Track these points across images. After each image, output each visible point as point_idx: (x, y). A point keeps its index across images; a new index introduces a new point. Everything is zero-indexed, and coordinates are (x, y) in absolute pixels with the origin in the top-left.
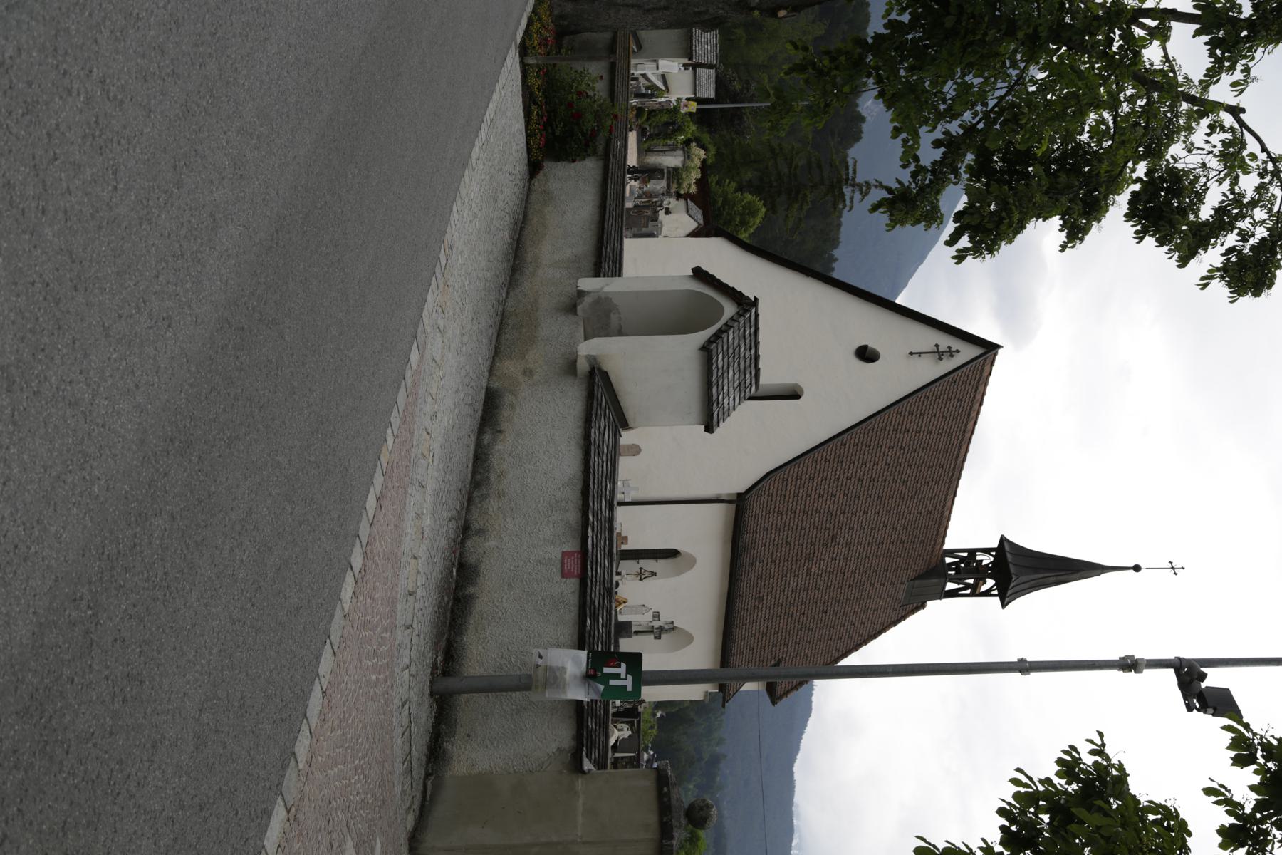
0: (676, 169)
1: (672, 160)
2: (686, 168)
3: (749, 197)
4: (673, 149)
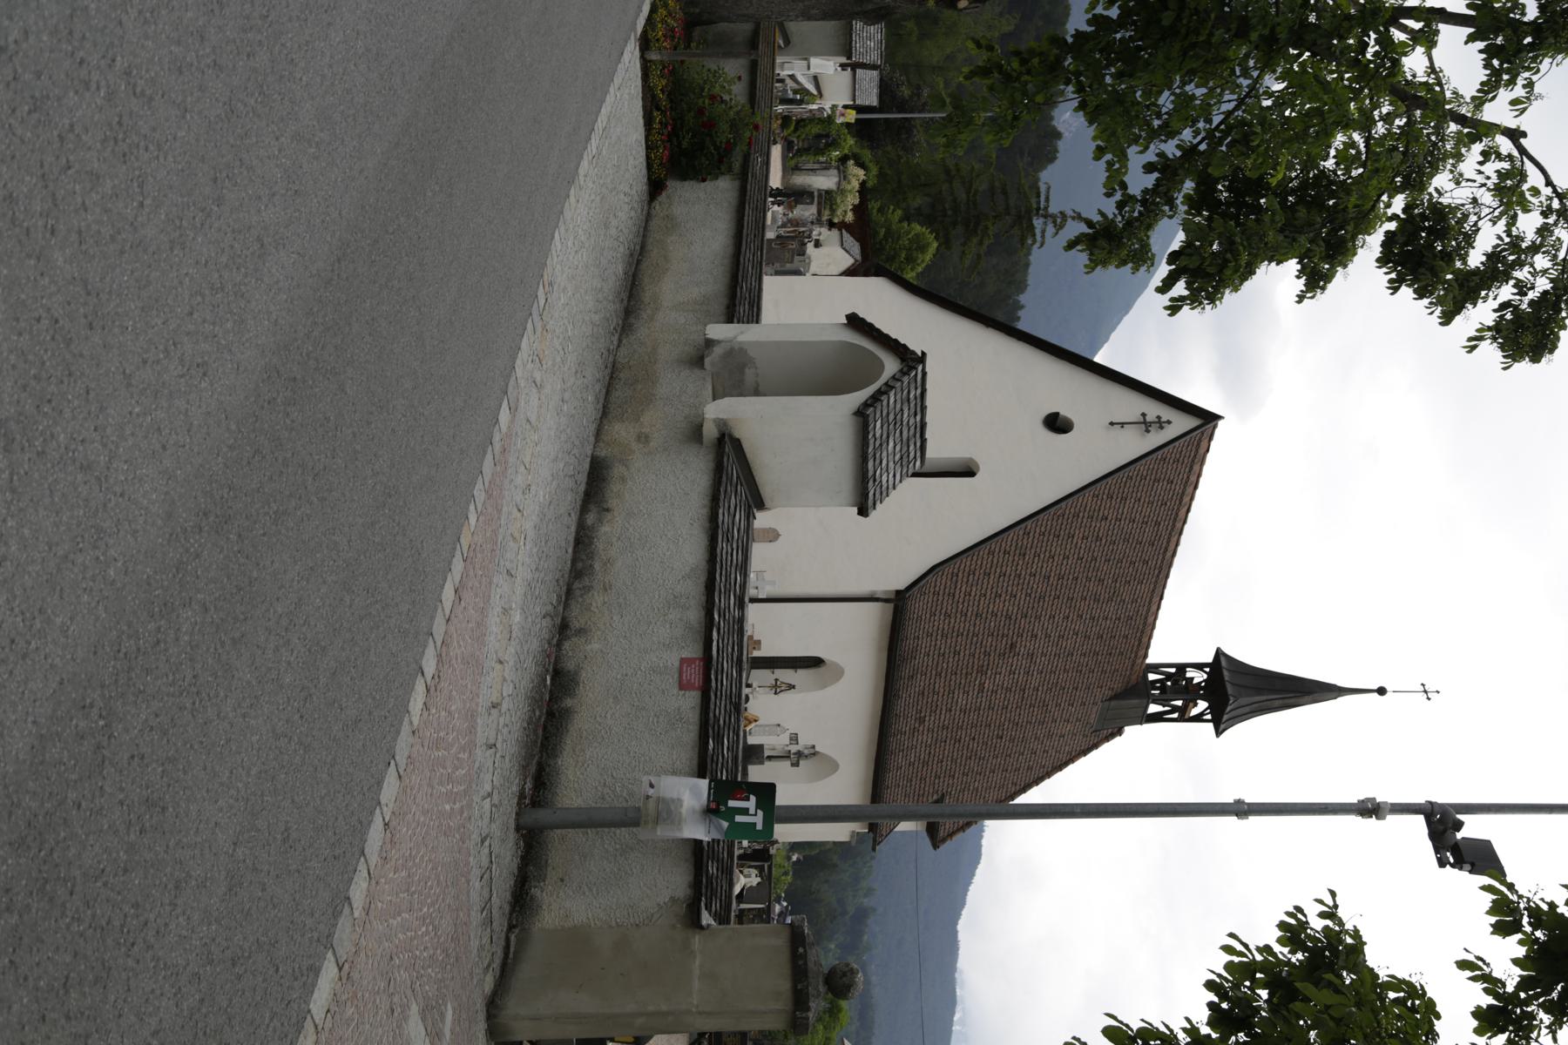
0: (828, 192)
1: (824, 181)
2: (841, 191)
3: (918, 228)
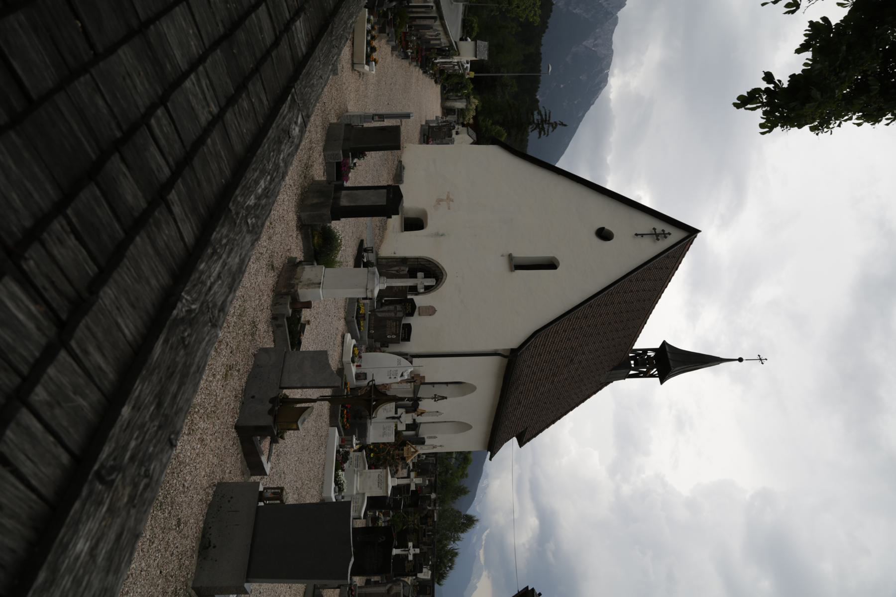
0: (462, 109)
1: (460, 105)
2: (467, 109)
3: (498, 128)
4: (461, 98)
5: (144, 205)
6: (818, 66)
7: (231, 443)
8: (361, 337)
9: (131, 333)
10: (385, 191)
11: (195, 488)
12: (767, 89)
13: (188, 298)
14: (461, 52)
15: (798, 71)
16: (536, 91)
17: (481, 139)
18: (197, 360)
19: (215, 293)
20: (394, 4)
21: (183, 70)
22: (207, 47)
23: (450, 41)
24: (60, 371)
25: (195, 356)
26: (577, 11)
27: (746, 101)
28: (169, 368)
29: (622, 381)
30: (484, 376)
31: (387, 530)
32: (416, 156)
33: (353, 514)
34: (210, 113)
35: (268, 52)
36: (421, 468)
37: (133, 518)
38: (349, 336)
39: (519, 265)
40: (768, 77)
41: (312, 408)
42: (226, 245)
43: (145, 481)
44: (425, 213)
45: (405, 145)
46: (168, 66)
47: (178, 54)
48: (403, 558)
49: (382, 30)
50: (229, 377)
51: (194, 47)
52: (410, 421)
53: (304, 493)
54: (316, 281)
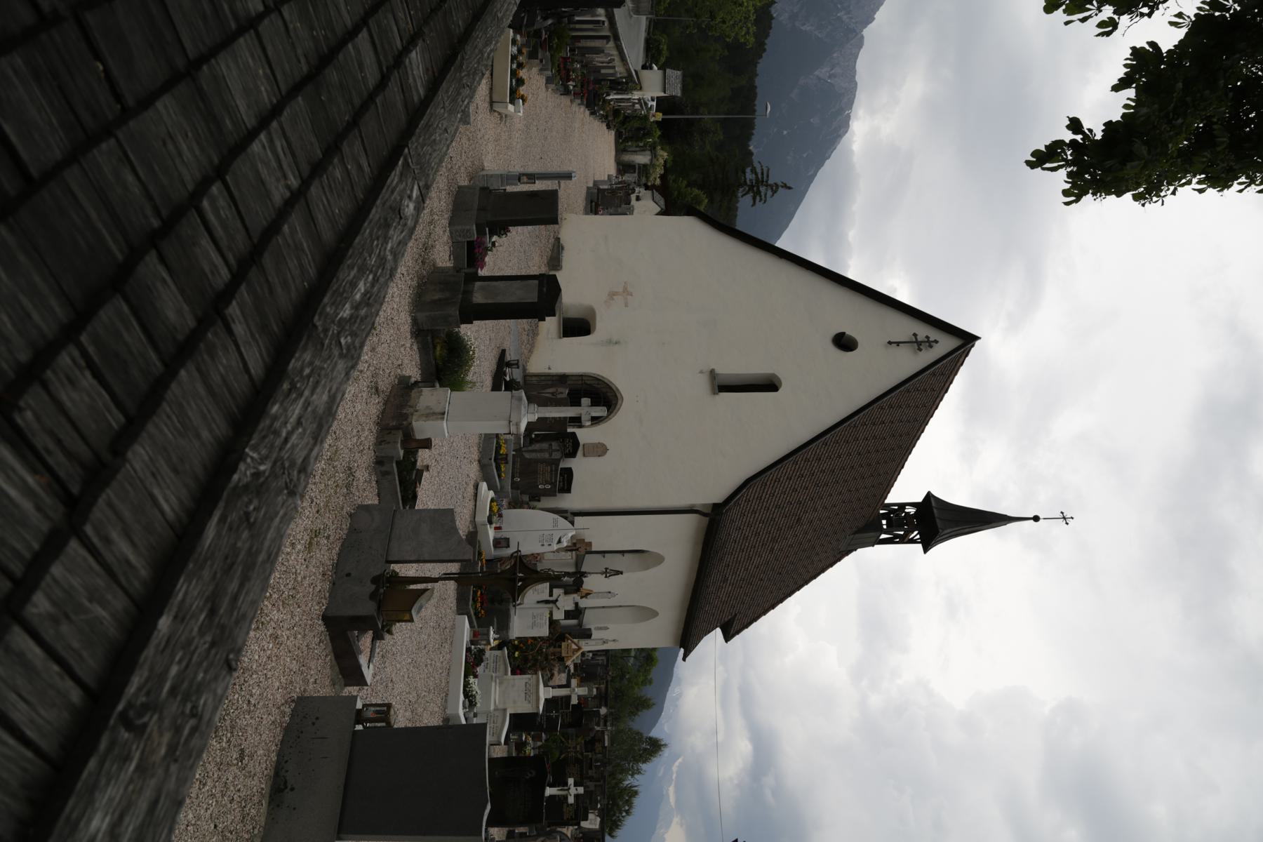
0: (645, 165)
1: (642, 159)
2: (652, 165)
3: (696, 191)
4: (643, 149)
5: (191, 323)
6: (1144, 110)
7: (317, 640)
8: (502, 487)
9: (173, 509)
10: (536, 282)
11: (266, 706)
12: (1073, 142)
13: (255, 455)
14: (645, 85)
15: (1116, 117)
16: (749, 139)
17: (671, 208)
18: (267, 544)
19: (294, 447)
20: (550, 22)
21: (249, 126)
22: (284, 93)
23: (628, 71)
24: (70, 570)
25: (265, 538)
26: (807, 28)
27: (1044, 158)
28: (226, 558)
29: (870, 548)
30: (675, 542)
31: (538, 761)
32: (580, 231)
33: (489, 739)
34: (288, 187)
35: (371, 97)
36: (586, 671)
37: (174, 779)
38: (484, 486)
39: (725, 386)
40: (1075, 125)
41: (433, 589)
42: (309, 376)
43: (192, 722)
44: (592, 312)
45: (565, 215)
46: (228, 122)
47: (242, 104)
48: (560, 801)
49: (533, 55)
50: (314, 546)
51: (265, 94)
52: (571, 607)
53: (420, 710)
54: (439, 410)
